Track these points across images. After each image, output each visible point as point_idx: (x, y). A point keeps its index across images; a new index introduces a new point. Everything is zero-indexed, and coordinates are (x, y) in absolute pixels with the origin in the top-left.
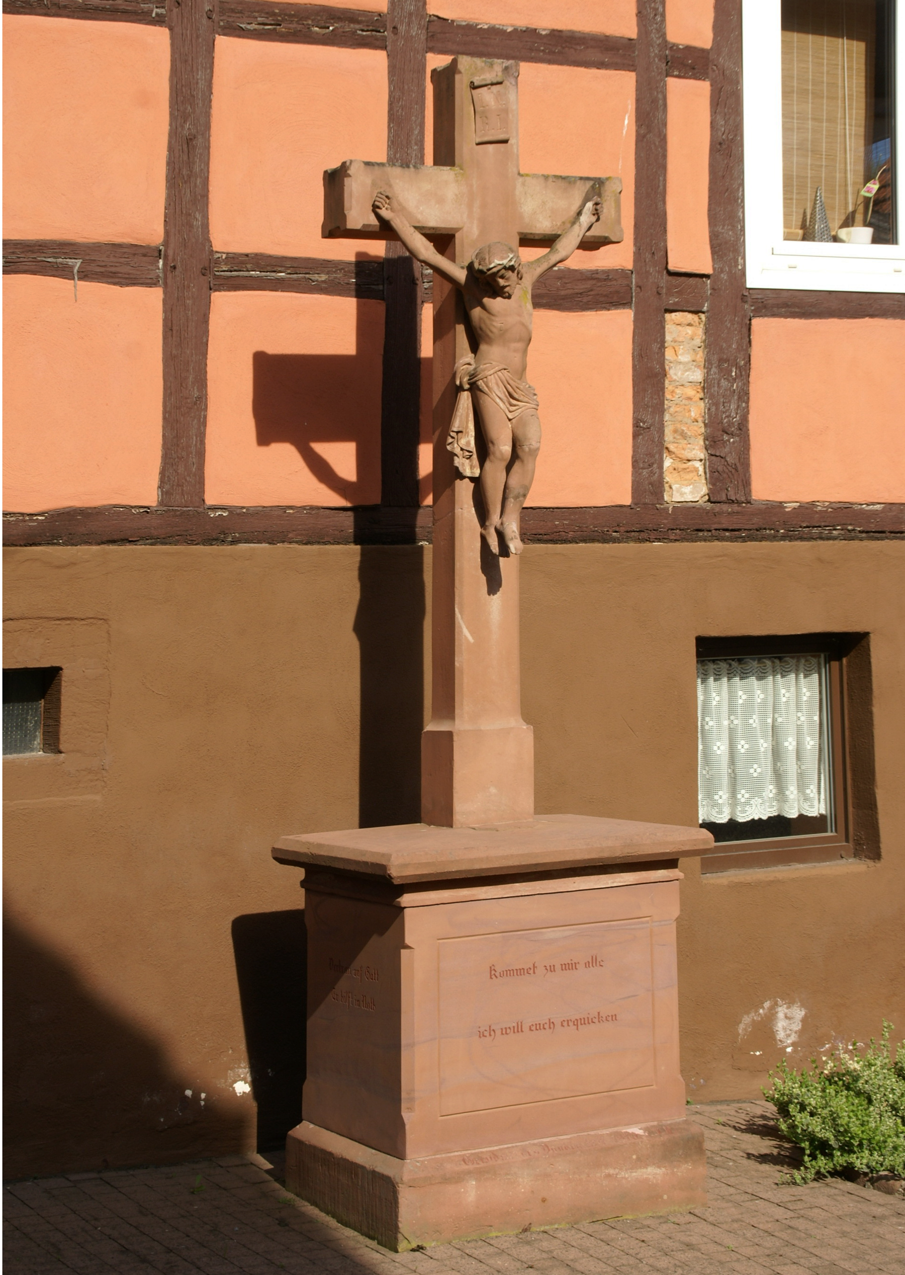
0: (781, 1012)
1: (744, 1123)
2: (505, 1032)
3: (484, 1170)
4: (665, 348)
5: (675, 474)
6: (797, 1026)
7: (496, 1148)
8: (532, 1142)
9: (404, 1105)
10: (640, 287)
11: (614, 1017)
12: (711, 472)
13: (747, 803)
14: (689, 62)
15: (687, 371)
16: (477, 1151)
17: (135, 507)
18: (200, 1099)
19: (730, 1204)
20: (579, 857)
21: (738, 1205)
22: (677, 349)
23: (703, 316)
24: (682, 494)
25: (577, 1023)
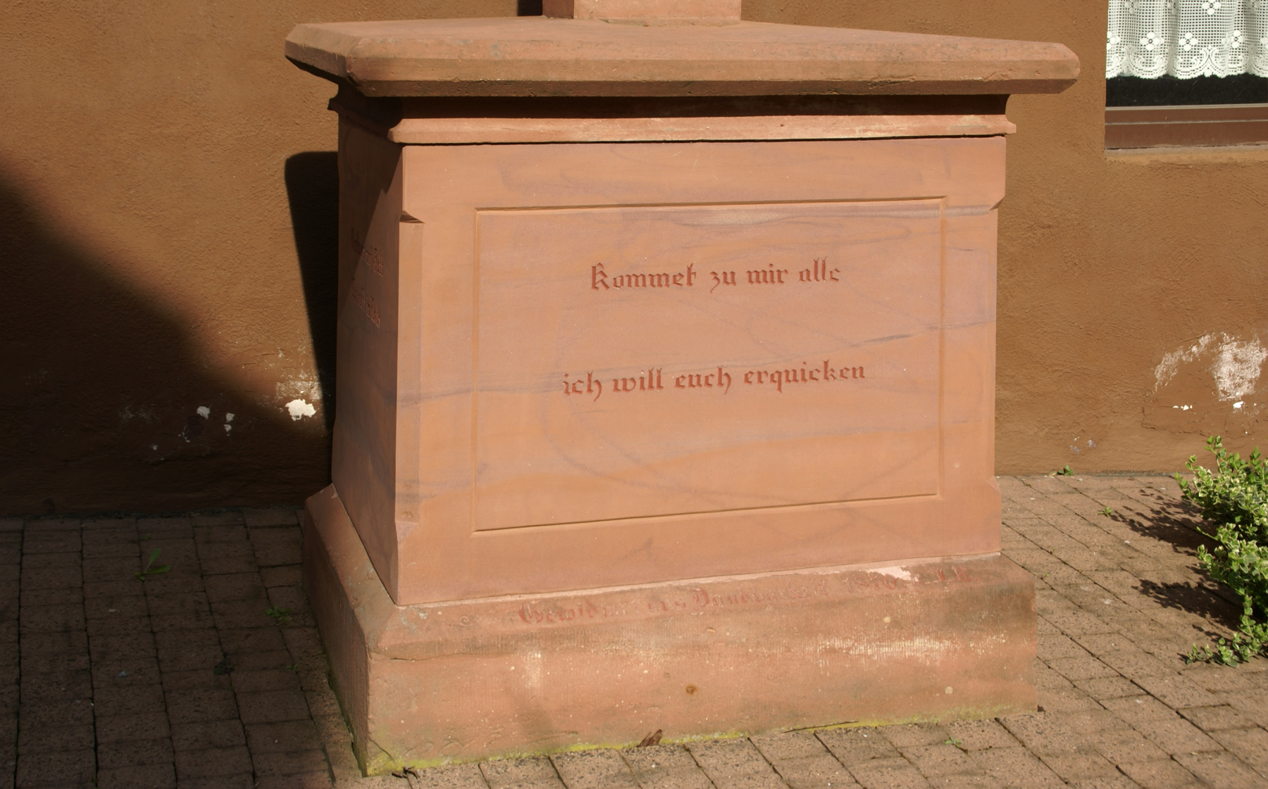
0: (1228, 352)
1: (1151, 515)
2: (622, 386)
3: (561, 631)
6: (1253, 373)
7: (596, 592)
8: (676, 583)
9: (399, 506)
11: (858, 372)
13: (1195, 52)
16: (554, 595)
18: (225, 422)
19: (1083, 704)
20: (783, 76)
21: (1099, 704)
25: (778, 379)
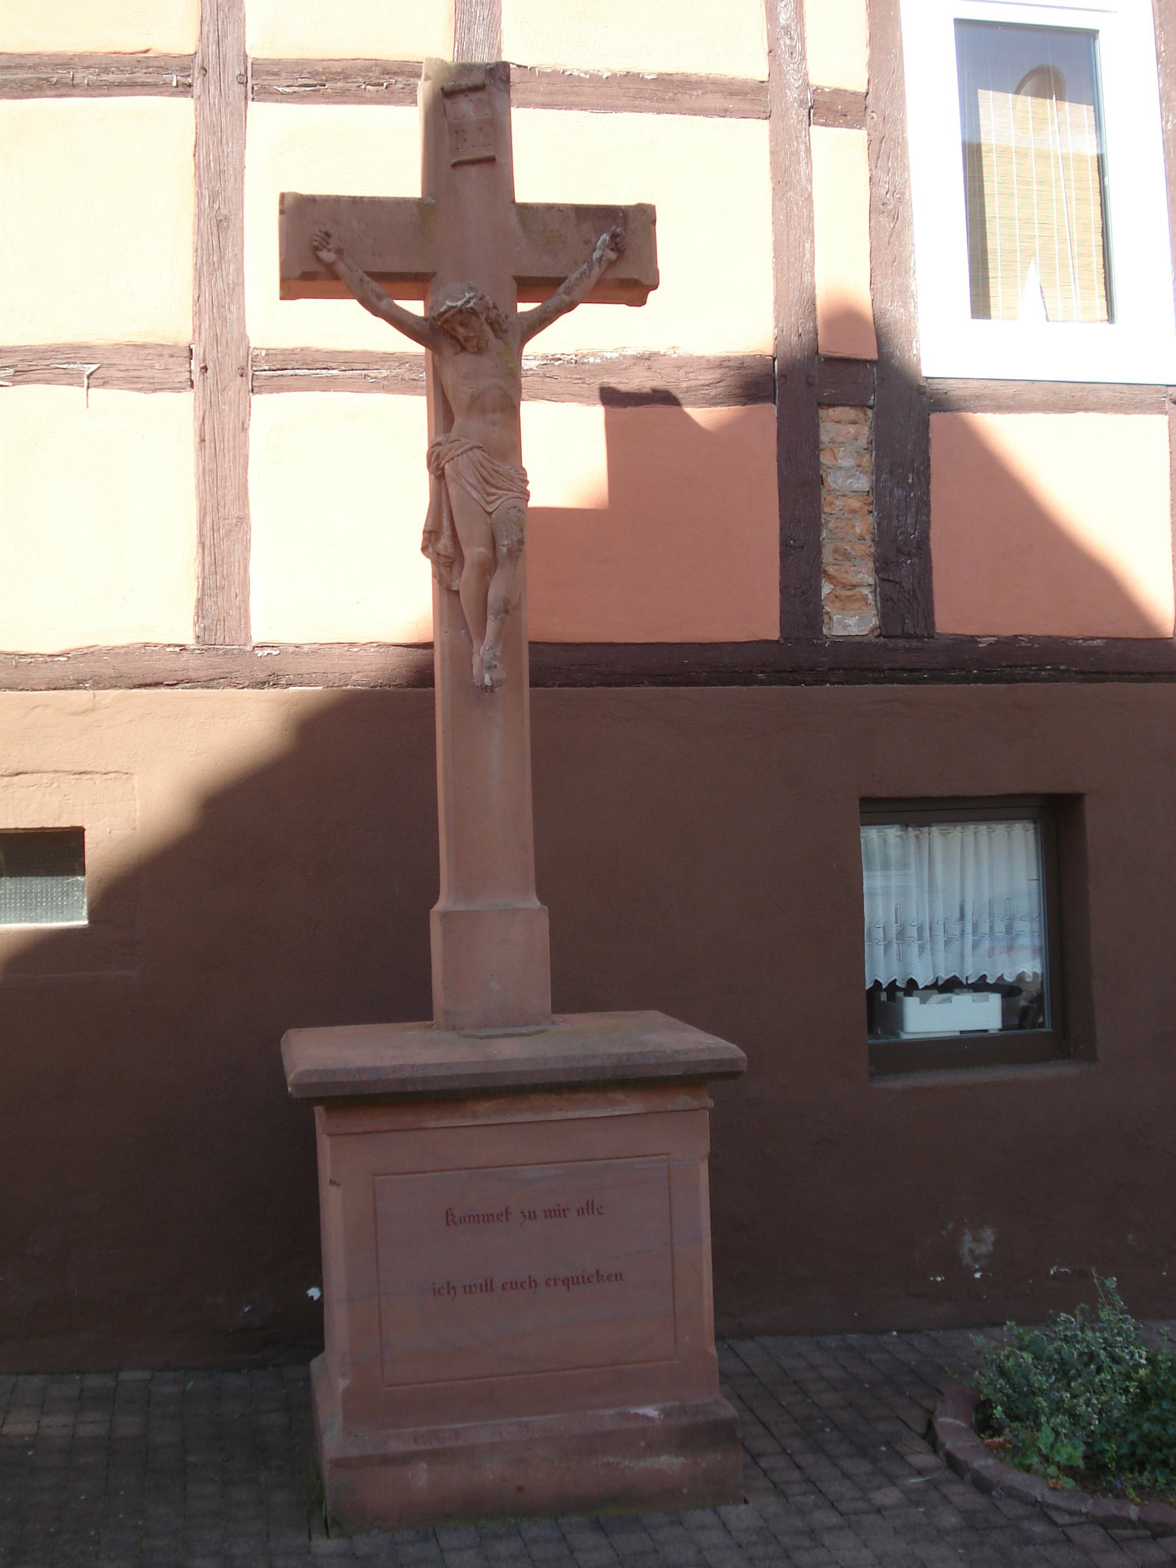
2: (468, 1289)
4: (820, 450)
5: (838, 604)
10: (785, 377)
11: (619, 1277)
12: (882, 599)
14: (833, 108)
15: (849, 478)
17: (169, 646)
22: (836, 451)
23: (870, 413)
24: (846, 626)
